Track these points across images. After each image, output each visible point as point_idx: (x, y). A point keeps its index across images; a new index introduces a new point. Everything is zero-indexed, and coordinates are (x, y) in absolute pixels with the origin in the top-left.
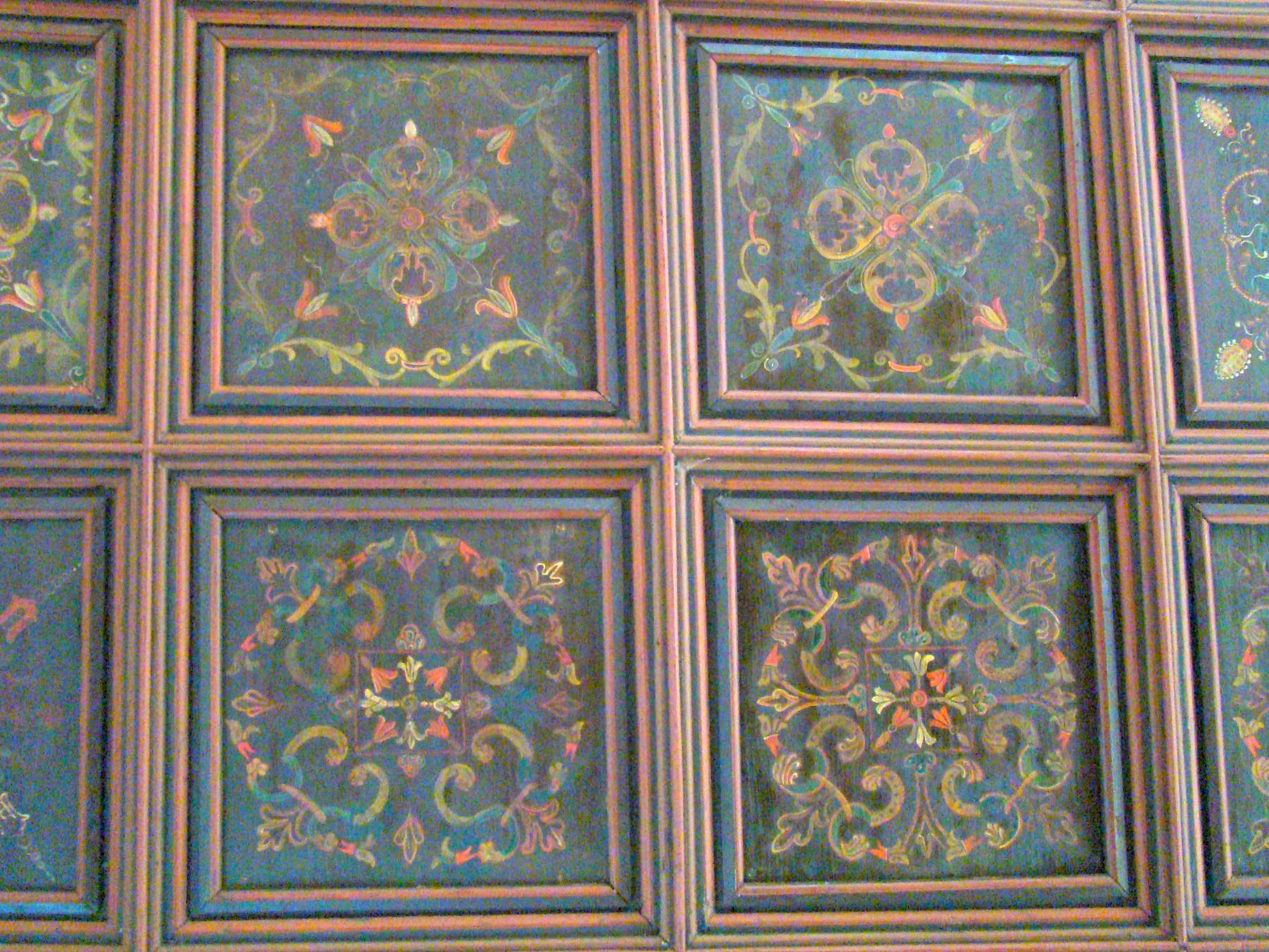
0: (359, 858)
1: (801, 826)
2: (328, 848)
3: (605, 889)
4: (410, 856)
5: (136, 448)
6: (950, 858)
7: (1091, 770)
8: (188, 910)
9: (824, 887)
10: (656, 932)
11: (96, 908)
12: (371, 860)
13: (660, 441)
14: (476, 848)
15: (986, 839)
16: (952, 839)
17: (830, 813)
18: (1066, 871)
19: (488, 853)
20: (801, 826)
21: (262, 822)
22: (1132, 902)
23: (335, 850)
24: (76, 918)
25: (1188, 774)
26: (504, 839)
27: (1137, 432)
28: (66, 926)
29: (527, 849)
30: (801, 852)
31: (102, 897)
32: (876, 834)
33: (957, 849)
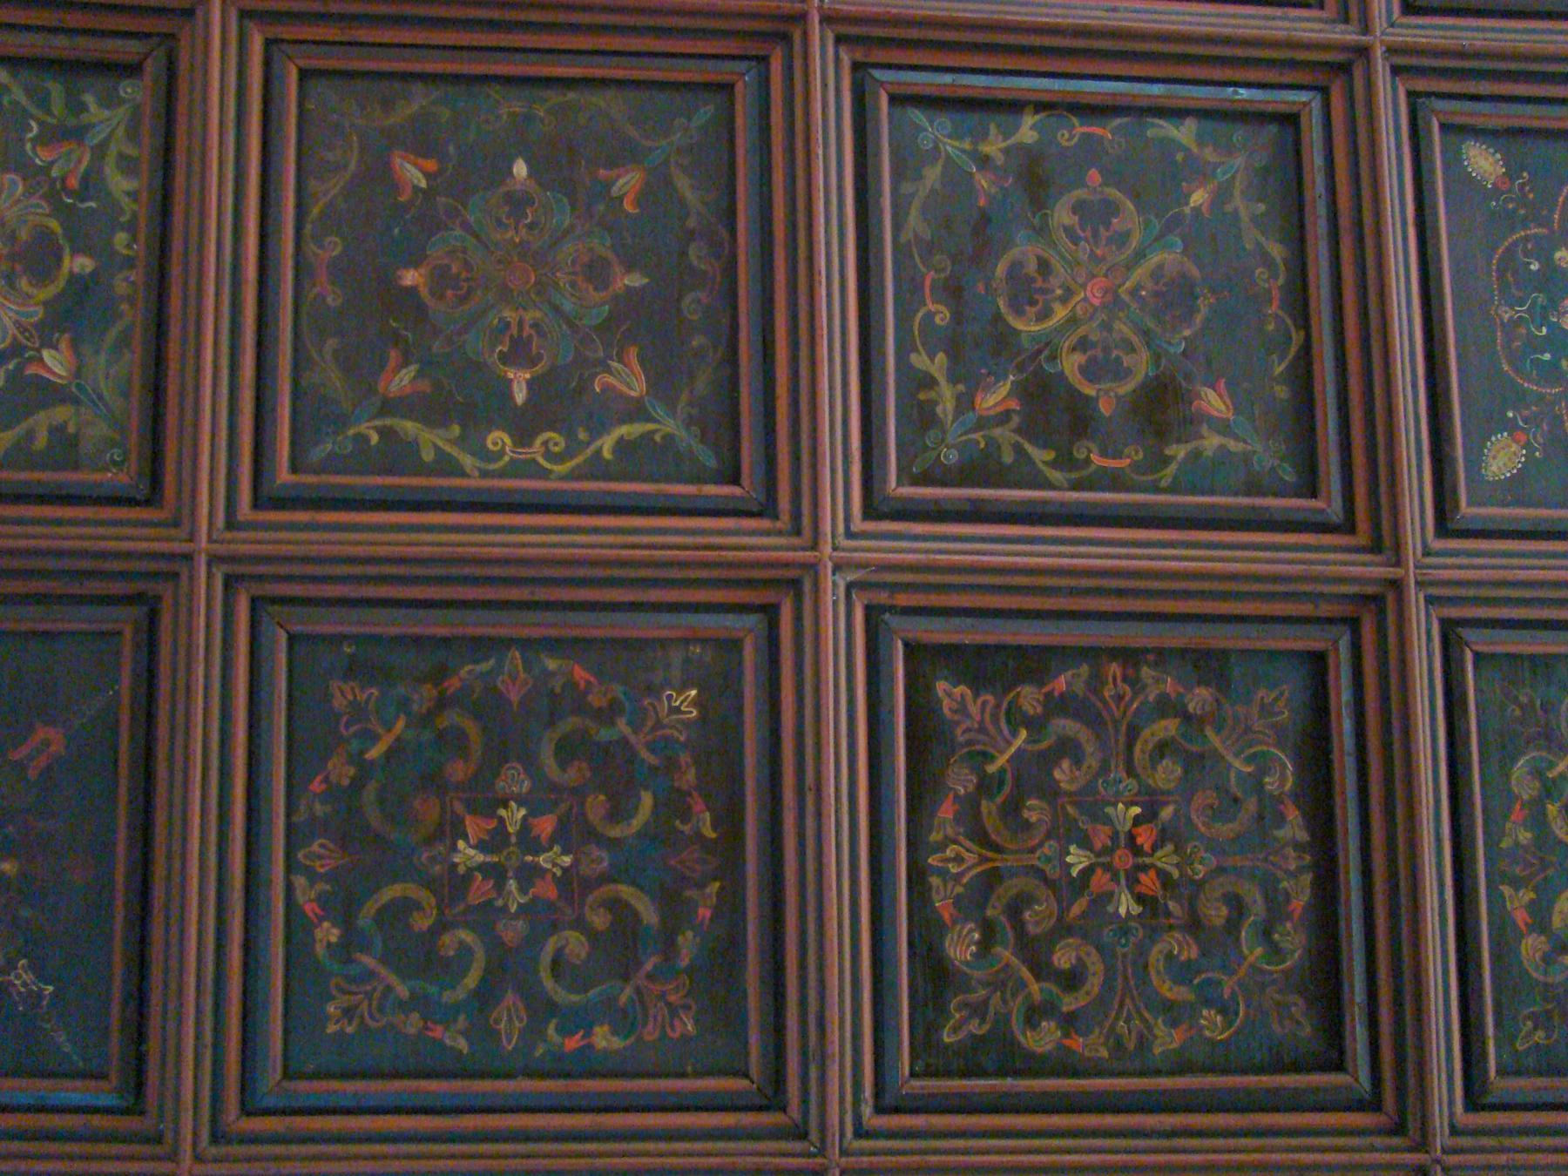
0: (448, 1042)
2: (412, 1031)
5: (185, 547)
6: (1157, 1050)
10: (803, 1135)
11: (132, 1099)
12: (462, 1044)
13: (822, 1151)
14: (589, 1032)
16: (1160, 1029)
17: (1014, 995)
18: (1296, 1068)
19: (603, 1038)
20: (979, 1010)
21: (333, 998)
24: (108, 1111)
28: (97, 1121)
29: (650, 1033)
30: (978, 1042)
31: (140, 1086)
32: (1070, 1022)
33: (1166, 1039)
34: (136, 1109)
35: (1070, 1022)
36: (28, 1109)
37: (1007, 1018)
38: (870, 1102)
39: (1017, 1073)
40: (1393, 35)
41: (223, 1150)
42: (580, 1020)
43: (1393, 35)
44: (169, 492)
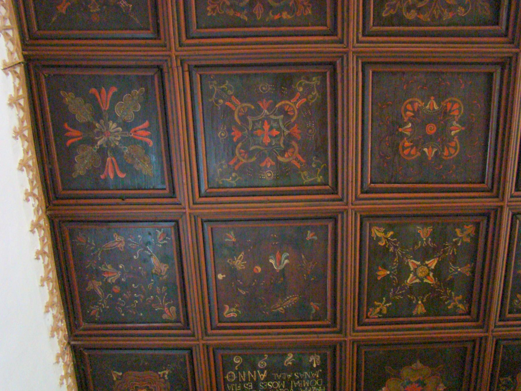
0: (242, 18)
1: (394, 7)
2: (232, 15)
3: (325, 28)
4: (259, 17)
6: (444, 19)
7: (485, 145)
8: (186, 36)
9: (401, 28)
10: (342, 42)
12: (246, 19)
13: (348, 46)
14: (281, 14)
15: (458, 13)
16: (446, 12)
17: (404, 2)
18: (485, 24)
19: (285, 15)
20: (394, 7)
21: (209, 5)
22: (506, 36)
23: (234, 15)
24: (151, 39)
25: (507, 231)
26: (291, 11)
27: (500, 195)
28: (148, 41)
29: (298, 14)
30: (392, 16)
31: (158, 32)
32: (419, 10)
33: (447, 16)
34: (158, 38)
35: (419, 10)
36: (130, 39)
37: (401, 9)
38: (361, 33)
39: (403, 25)
40: (497, 331)
41: (183, 48)
42: (278, 11)
43: (497, 331)
44: (191, 325)
